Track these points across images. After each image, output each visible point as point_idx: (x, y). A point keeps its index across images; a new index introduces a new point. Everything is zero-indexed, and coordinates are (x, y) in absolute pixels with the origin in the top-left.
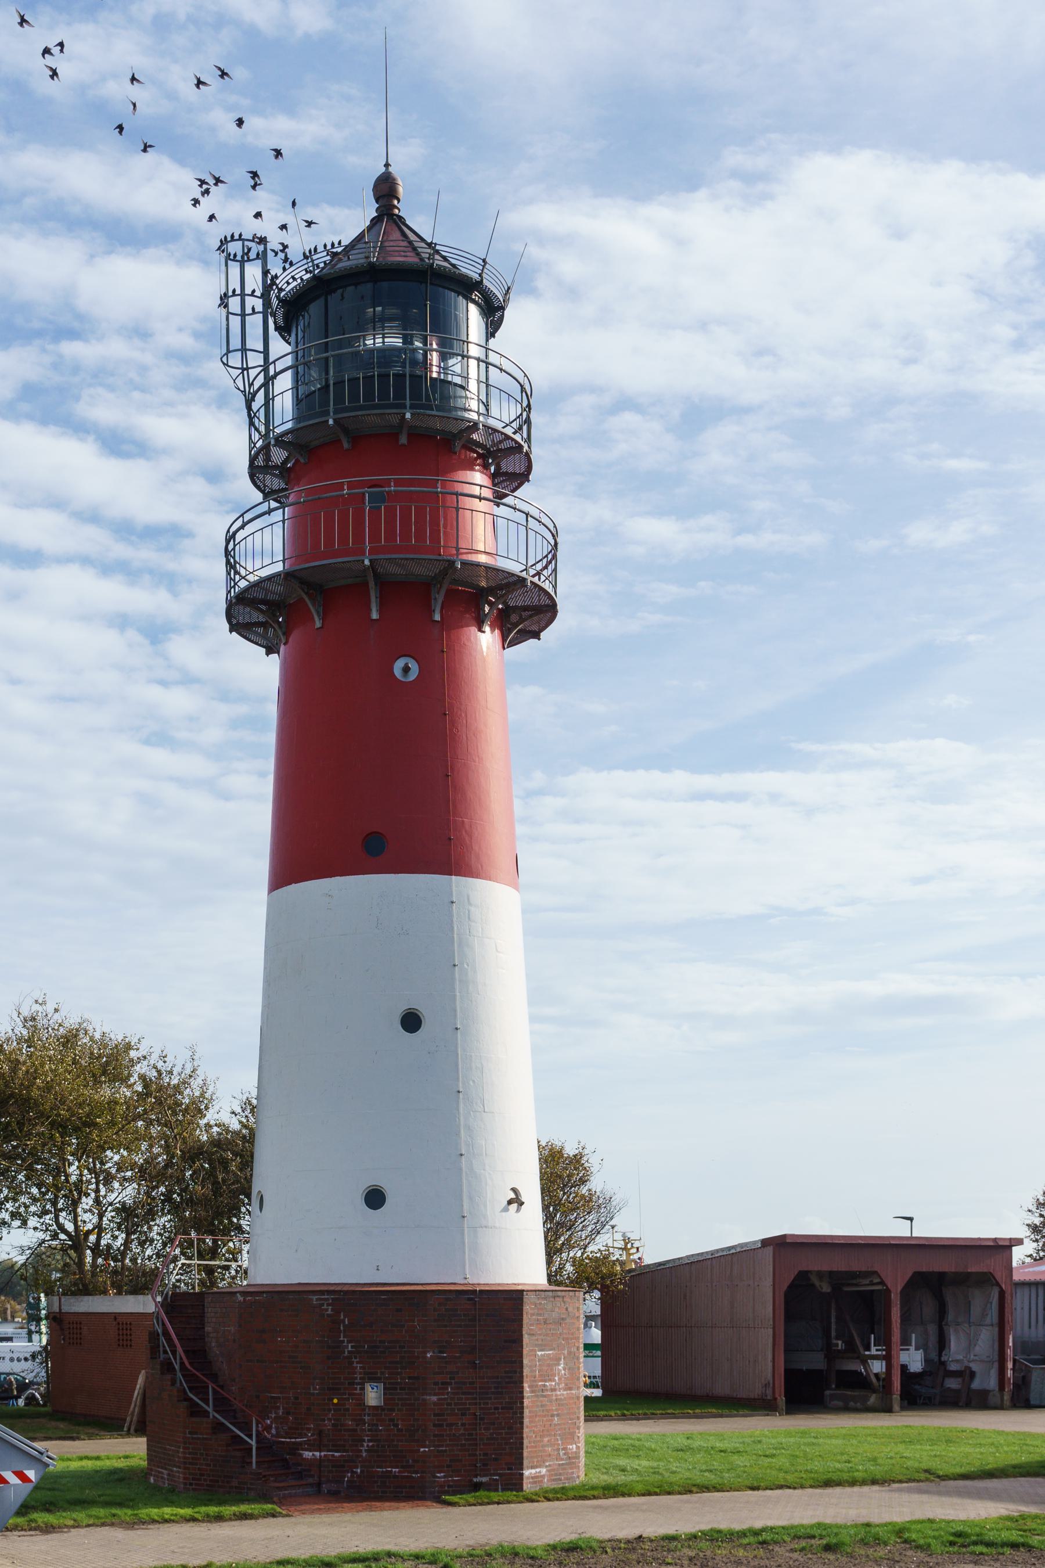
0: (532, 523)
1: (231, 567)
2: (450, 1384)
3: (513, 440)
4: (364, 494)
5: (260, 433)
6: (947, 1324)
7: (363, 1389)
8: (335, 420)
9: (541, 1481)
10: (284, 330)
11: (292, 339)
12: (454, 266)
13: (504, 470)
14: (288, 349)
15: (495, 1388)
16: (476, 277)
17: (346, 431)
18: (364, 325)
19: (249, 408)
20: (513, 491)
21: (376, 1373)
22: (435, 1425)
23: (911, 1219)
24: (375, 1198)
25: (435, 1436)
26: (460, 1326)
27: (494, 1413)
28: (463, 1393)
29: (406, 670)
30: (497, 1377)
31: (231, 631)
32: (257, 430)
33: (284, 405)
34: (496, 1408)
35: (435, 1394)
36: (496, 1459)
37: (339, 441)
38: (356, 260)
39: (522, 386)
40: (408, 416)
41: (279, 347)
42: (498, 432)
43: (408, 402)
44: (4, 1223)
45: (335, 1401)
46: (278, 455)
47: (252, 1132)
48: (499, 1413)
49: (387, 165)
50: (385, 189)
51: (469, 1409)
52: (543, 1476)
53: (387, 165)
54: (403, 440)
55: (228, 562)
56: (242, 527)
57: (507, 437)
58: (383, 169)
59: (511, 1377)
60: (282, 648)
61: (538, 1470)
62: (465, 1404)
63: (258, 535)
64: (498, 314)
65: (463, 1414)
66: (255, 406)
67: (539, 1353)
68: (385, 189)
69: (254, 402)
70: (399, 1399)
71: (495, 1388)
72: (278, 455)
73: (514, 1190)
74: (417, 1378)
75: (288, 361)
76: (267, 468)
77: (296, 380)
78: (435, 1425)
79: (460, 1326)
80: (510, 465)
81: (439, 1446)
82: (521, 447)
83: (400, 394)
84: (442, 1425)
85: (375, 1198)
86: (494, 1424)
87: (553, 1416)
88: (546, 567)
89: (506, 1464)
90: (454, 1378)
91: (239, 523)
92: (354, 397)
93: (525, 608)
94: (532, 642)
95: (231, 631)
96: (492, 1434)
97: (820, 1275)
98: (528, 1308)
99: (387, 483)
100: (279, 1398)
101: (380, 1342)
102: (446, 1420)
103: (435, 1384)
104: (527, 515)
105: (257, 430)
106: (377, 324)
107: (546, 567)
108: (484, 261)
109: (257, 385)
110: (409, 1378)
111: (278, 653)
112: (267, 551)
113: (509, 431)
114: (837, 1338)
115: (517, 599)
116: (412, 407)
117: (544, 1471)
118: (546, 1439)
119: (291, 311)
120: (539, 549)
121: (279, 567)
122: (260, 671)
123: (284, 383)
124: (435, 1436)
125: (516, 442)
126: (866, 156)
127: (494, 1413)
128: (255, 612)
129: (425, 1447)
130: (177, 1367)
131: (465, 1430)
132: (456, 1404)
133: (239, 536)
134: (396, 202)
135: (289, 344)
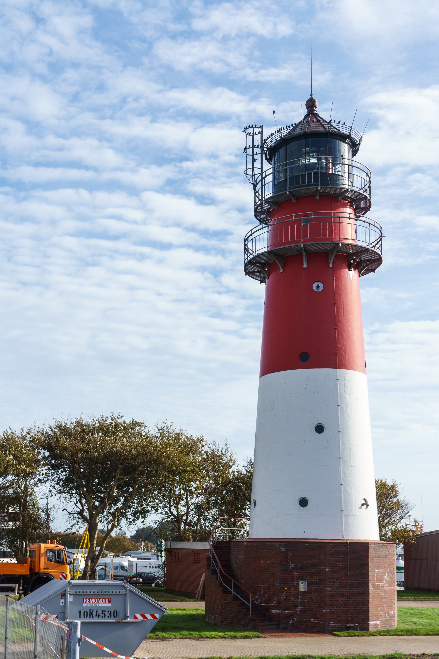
1: (246, 250)
2: (337, 582)
3: (363, 195)
4: (301, 219)
5: (259, 199)
7: (298, 584)
8: (289, 192)
9: (378, 627)
10: (269, 160)
11: (272, 163)
12: (339, 130)
13: (359, 206)
14: (271, 166)
16: (348, 134)
18: (301, 156)
19: (255, 189)
20: (363, 215)
24: (304, 503)
26: (341, 558)
27: (356, 596)
28: (342, 587)
29: (318, 287)
30: (357, 580)
31: (246, 275)
32: (258, 197)
33: (268, 193)
34: (357, 594)
36: (357, 616)
37: (291, 200)
38: (298, 131)
39: (367, 174)
41: (267, 166)
42: (357, 192)
43: (319, 183)
45: (286, 589)
46: (266, 207)
47: (251, 477)
49: (311, 95)
50: (311, 104)
52: (378, 625)
53: (311, 95)
54: (317, 198)
55: (245, 248)
56: (251, 235)
57: (361, 194)
58: (310, 97)
59: (364, 581)
60: (267, 281)
61: (376, 622)
62: (343, 592)
63: (257, 249)
65: (342, 596)
67: (376, 570)
68: (311, 104)
69: (257, 184)
70: (314, 589)
72: (266, 207)
73: (364, 499)
75: (271, 171)
76: (262, 212)
78: (329, 601)
80: (362, 204)
82: (366, 197)
83: (316, 180)
84: (333, 601)
85: (304, 503)
86: (356, 601)
88: (377, 244)
91: (250, 233)
92: (297, 182)
93: (368, 260)
95: (246, 275)
96: (355, 605)
98: (371, 551)
99: (311, 215)
100: (261, 586)
101: (306, 564)
104: (369, 224)
105: (258, 197)
106: (307, 154)
107: (377, 244)
108: (351, 127)
112: (261, 245)
113: (361, 192)
115: (365, 257)
117: (379, 622)
119: (272, 152)
120: (374, 237)
121: (266, 250)
122: (258, 289)
123: (269, 179)
124: (330, 605)
127: (356, 596)
128: (256, 267)
130: (218, 572)
131: (343, 603)
132: (339, 592)
133: (250, 239)
134: (315, 108)
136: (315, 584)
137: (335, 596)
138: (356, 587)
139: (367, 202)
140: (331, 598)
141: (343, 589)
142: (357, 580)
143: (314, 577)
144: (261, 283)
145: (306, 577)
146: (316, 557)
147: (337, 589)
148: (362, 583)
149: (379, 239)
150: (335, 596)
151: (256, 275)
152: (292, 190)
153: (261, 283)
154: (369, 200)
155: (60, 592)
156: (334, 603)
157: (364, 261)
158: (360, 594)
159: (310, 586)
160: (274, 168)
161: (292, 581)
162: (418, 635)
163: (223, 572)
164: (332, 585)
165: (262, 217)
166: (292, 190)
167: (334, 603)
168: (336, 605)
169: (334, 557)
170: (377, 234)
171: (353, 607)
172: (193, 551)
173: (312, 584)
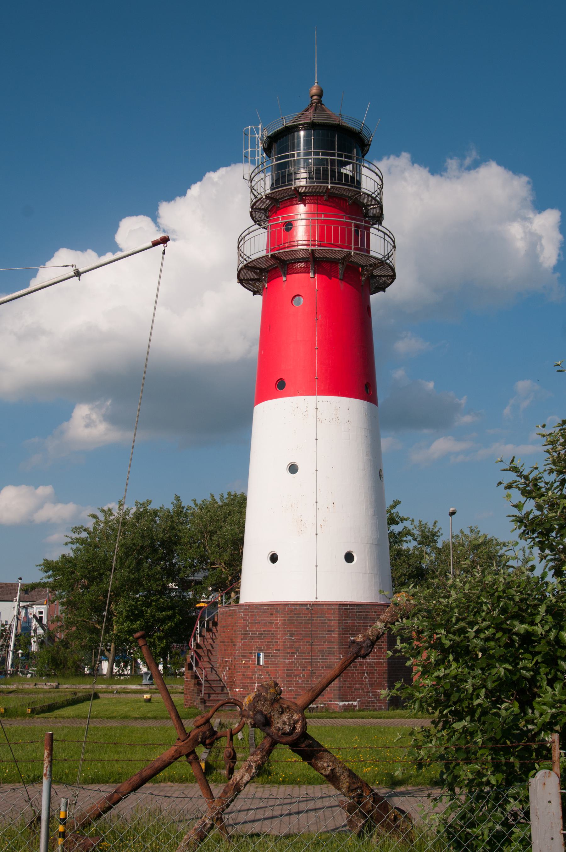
0: (386, 237)
2: (296, 653)
15: (322, 656)
25: (287, 681)
26: (302, 623)
28: (303, 659)
30: (323, 651)
31: (384, 291)
34: (322, 667)
35: (287, 659)
40: (329, 187)
44: (500, 839)
45: (244, 662)
51: (307, 667)
52: (355, 706)
55: (239, 252)
56: (249, 234)
61: (350, 703)
64: (367, 147)
65: (304, 670)
71: (322, 656)
79: (302, 623)
81: (289, 687)
85: (274, 558)
89: (328, 698)
94: (381, 293)
102: (293, 673)
104: (385, 233)
110: (276, 650)
116: (331, 183)
117: (355, 703)
124: (287, 681)
126: (96, 254)
130: (194, 665)
131: (304, 678)
132: (299, 664)
133: (246, 238)
141: (305, 662)
142: (323, 651)
144: (254, 294)
145: (264, 647)
151: (251, 284)
153: (254, 294)
155: (398, 712)
158: (326, 667)
162: (376, 718)
168: (295, 681)
170: (376, 184)
173: (269, 656)
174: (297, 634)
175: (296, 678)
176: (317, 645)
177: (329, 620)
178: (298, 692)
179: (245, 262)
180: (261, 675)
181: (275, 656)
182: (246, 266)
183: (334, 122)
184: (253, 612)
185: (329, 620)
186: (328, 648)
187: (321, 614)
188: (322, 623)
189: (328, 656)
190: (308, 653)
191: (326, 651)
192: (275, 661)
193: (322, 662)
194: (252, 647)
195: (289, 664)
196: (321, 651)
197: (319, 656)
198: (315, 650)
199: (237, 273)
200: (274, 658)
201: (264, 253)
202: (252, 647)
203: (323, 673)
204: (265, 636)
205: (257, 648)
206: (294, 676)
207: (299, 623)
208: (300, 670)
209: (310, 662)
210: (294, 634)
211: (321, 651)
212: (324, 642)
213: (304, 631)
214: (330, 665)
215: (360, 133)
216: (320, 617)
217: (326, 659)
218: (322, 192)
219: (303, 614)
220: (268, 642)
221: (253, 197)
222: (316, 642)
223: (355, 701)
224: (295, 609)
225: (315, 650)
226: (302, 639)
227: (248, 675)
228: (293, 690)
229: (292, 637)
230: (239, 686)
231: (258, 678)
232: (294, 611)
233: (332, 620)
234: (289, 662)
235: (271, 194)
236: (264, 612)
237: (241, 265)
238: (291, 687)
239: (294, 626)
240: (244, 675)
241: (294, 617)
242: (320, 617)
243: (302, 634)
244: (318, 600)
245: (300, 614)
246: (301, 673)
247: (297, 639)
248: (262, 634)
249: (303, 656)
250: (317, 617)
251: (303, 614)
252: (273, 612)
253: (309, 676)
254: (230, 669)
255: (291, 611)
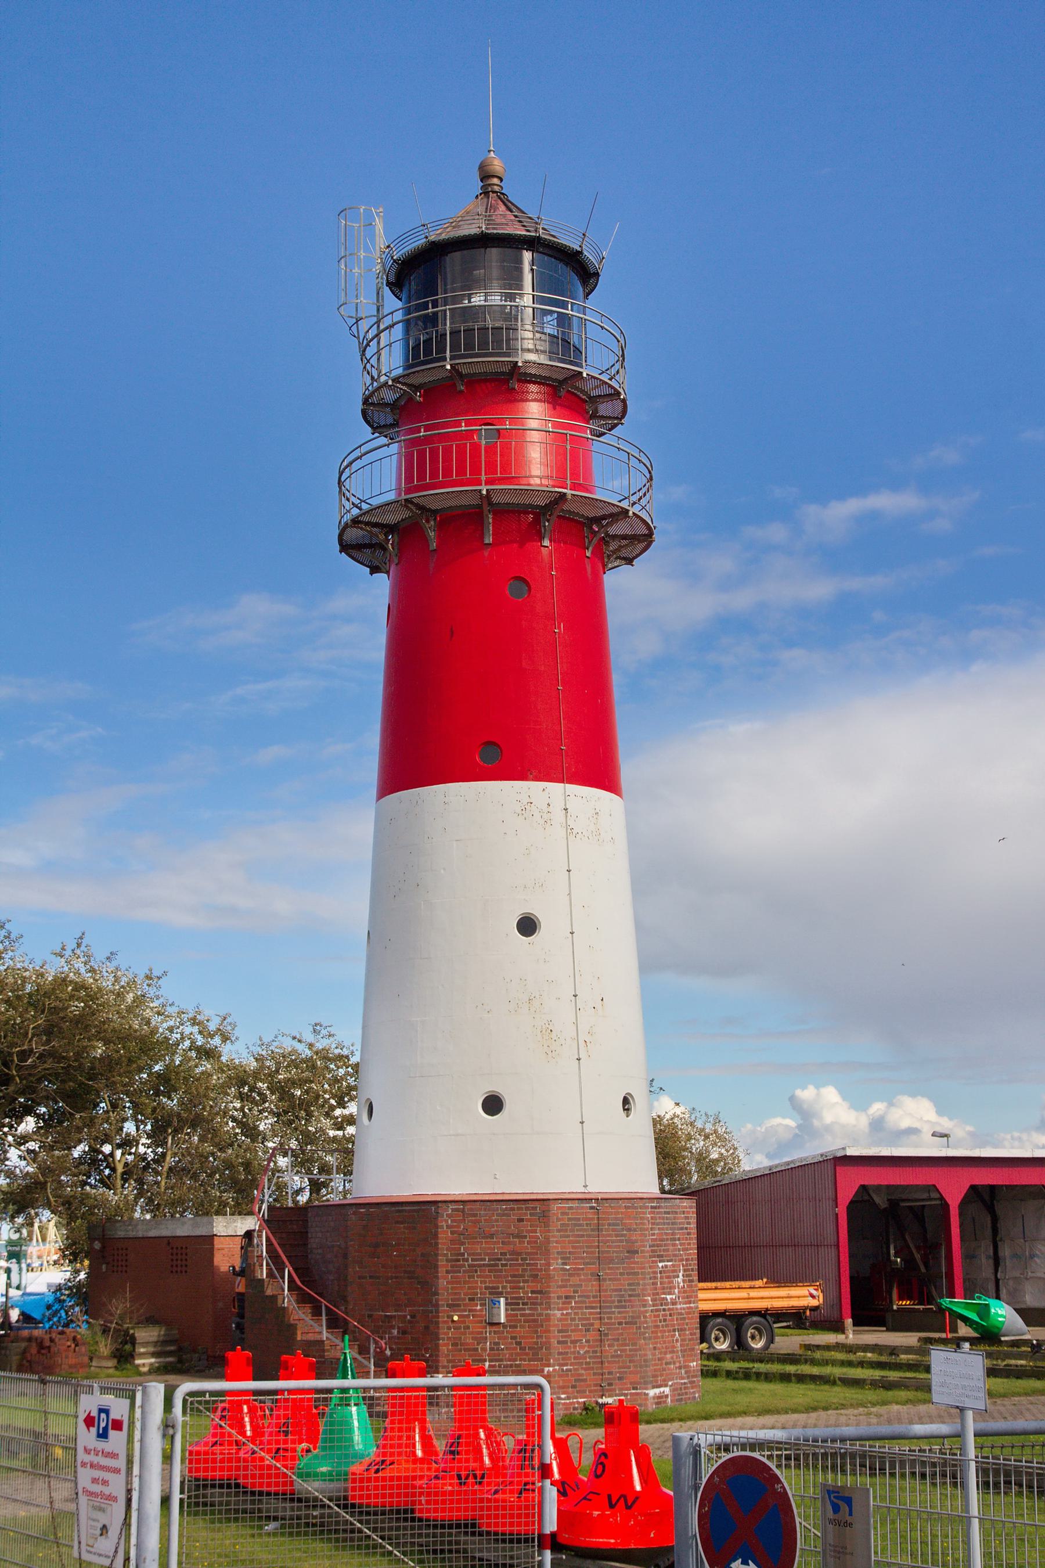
3: (610, 386)
6: (1001, 1240)
9: (665, 1402)
11: (404, 296)
14: (399, 304)
15: (619, 1301)
17: (460, 374)
20: (610, 430)
21: (460, 1294)
22: (559, 1342)
23: (946, 1136)
25: (559, 1354)
26: (582, 1236)
27: (618, 1329)
28: (586, 1308)
30: (620, 1290)
31: (371, 574)
33: (392, 361)
34: (620, 1323)
36: (620, 1378)
41: (392, 303)
42: (595, 378)
48: (623, 1329)
51: (592, 1325)
52: (667, 1396)
56: (360, 458)
59: (634, 1290)
61: (662, 1389)
62: (589, 1319)
65: (588, 1330)
66: (369, 353)
67: (660, 1265)
70: (522, 1315)
71: (619, 1301)
74: (540, 1292)
77: (407, 331)
78: (559, 1342)
82: (619, 394)
84: (566, 1342)
86: (618, 1340)
87: (674, 1330)
90: (577, 1292)
92: (469, 346)
93: (624, 537)
95: (371, 574)
96: (616, 1351)
97: (878, 1188)
99: (458, 424)
100: (395, 1316)
101: (501, 1254)
102: (570, 1336)
103: (559, 1298)
109: (370, 336)
111: (388, 573)
113: (605, 378)
114: (896, 1256)
115: (619, 528)
117: (667, 1390)
118: (668, 1356)
124: (559, 1354)
125: (615, 389)
127: (618, 1329)
128: (366, 540)
129: (549, 1366)
133: (355, 466)
135: (400, 300)
136: (523, 1304)
137: (572, 1331)
138: (617, 1307)
139: (621, 404)
140: (562, 1337)
141: (590, 1313)
142: (620, 1290)
143: (523, 1288)
146: (525, 1237)
147: (575, 1314)
148: (630, 1296)
149: (644, 490)
150: (572, 1331)
152: (457, 361)
154: (624, 401)
156: (569, 1347)
157: (614, 537)
159: (512, 1310)
160: (408, 311)
161: (470, 1299)
163: (299, 1283)
164: (564, 1303)
165: (376, 419)
166: (457, 361)
167: (569, 1347)
168: (574, 1353)
169: (568, 1236)
171: (613, 1356)
172: (169, 1243)
173: (518, 1304)
174: (576, 1258)
175: (575, 1347)
176: (610, 1279)
177: (629, 1230)
178: (580, 1375)
179: (355, 512)
180: (498, 1344)
181: (532, 1304)
182: (356, 522)
183: (495, 231)
184: (475, 1215)
185: (629, 1230)
186: (629, 1285)
187: (616, 1219)
188: (617, 1236)
189: (630, 1301)
190: (594, 1297)
191: (625, 1290)
192: (533, 1315)
193: (619, 1313)
194: (476, 1288)
195: (560, 1320)
196: (616, 1290)
197: (613, 1302)
198: (606, 1291)
199: (337, 532)
200: (530, 1309)
201: (391, 496)
202: (476, 1288)
203: (622, 1334)
204: (506, 1265)
205: (486, 1288)
206: (572, 1342)
207: (578, 1236)
208: (581, 1330)
209: (597, 1313)
210: (569, 1258)
211: (616, 1290)
212: (621, 1274)
213: (587, 1253)
214: (633, 1317)
215: (581, 253)
216: (614, 1225)
217: (625, 1307)
218: (503, 373)
219: (583, 1219)
220: (513, 1276)
221: (368, 381)
222: (606, 1274)
223: (666, 1386)
224: (570, 1208)
225: (606, 1291)
226: (583, 1269)
227: (468, 1344)
228: (570, 1370)
229: (565, 1264)
230: (444, 1367)
231: (491, 1349)
232: (567, 1214)
233: (635, 1230)
234: (562, 1314)
235: (404, 376)
236: (503, 1215)
237: (347, 518)
238: (566, 1365)
239: (569, 1242)
240: (455, 1345)
241: (568, 1225)
242: (614, 1225)
243: (583, 1258)
244: (590, 1189)
245: (579, 1219)
246: (585, 1336)
247: (575, 1269)
248: (500, 1260)
249: (585, 1302)
250: (609, 1225)
251: (583, 1219)
252: (526, 1214)
253: (597, 1340)
254: (403, 1332)
255: (563, 1214)
